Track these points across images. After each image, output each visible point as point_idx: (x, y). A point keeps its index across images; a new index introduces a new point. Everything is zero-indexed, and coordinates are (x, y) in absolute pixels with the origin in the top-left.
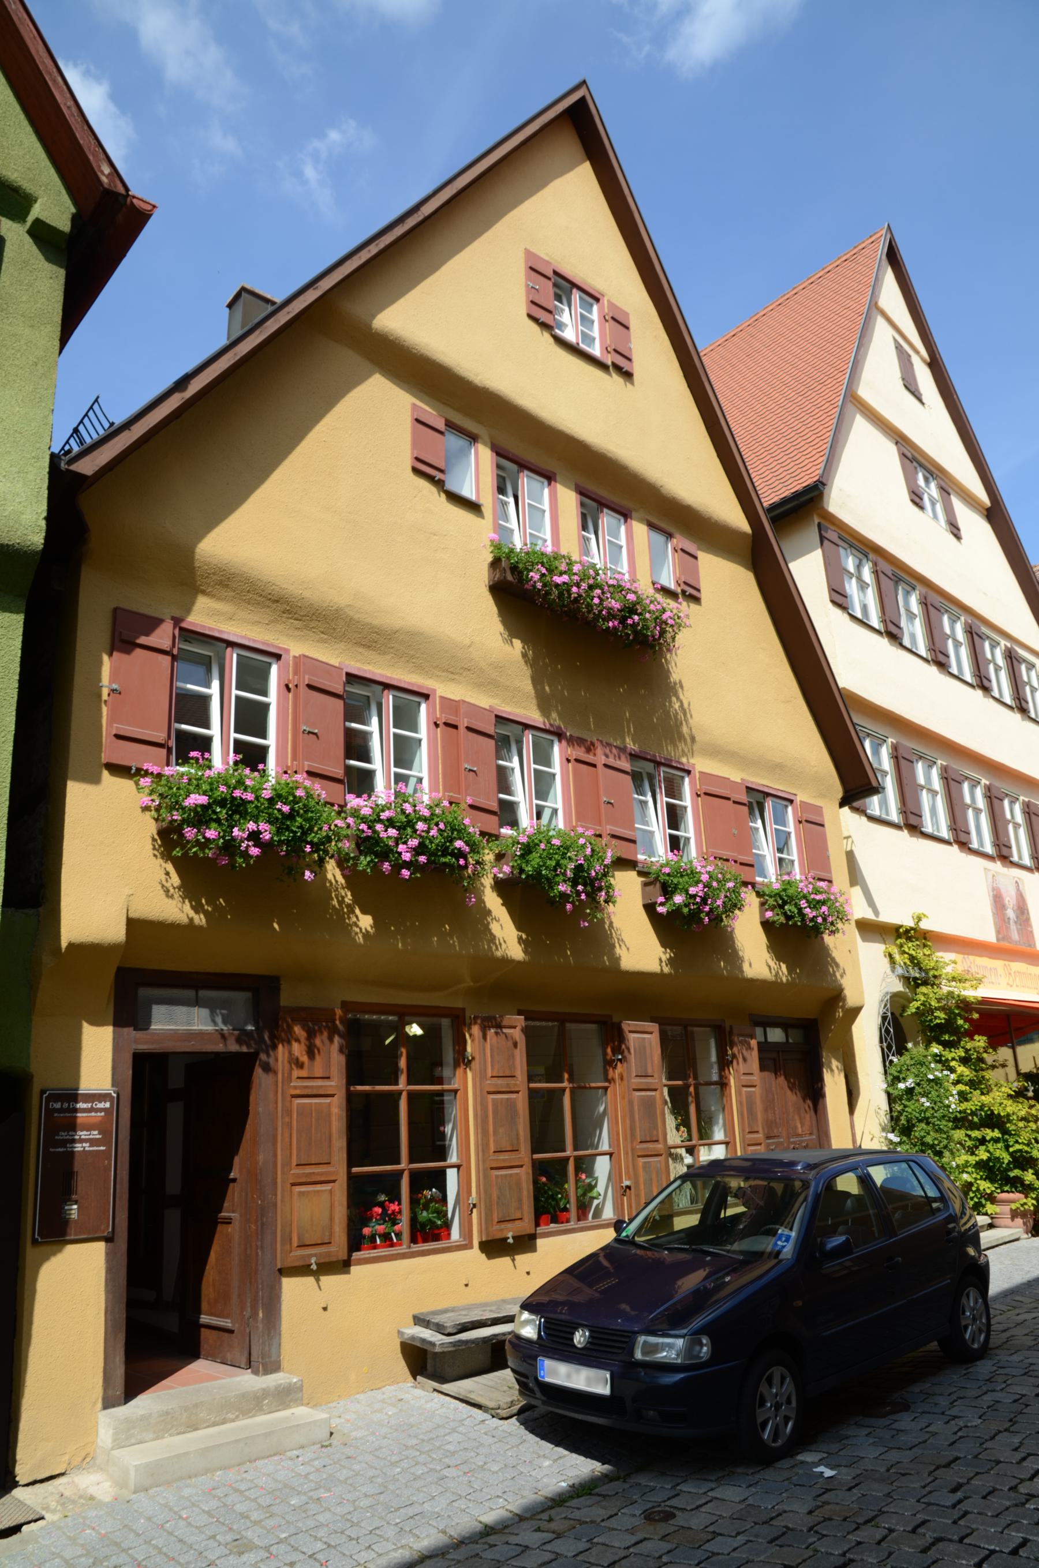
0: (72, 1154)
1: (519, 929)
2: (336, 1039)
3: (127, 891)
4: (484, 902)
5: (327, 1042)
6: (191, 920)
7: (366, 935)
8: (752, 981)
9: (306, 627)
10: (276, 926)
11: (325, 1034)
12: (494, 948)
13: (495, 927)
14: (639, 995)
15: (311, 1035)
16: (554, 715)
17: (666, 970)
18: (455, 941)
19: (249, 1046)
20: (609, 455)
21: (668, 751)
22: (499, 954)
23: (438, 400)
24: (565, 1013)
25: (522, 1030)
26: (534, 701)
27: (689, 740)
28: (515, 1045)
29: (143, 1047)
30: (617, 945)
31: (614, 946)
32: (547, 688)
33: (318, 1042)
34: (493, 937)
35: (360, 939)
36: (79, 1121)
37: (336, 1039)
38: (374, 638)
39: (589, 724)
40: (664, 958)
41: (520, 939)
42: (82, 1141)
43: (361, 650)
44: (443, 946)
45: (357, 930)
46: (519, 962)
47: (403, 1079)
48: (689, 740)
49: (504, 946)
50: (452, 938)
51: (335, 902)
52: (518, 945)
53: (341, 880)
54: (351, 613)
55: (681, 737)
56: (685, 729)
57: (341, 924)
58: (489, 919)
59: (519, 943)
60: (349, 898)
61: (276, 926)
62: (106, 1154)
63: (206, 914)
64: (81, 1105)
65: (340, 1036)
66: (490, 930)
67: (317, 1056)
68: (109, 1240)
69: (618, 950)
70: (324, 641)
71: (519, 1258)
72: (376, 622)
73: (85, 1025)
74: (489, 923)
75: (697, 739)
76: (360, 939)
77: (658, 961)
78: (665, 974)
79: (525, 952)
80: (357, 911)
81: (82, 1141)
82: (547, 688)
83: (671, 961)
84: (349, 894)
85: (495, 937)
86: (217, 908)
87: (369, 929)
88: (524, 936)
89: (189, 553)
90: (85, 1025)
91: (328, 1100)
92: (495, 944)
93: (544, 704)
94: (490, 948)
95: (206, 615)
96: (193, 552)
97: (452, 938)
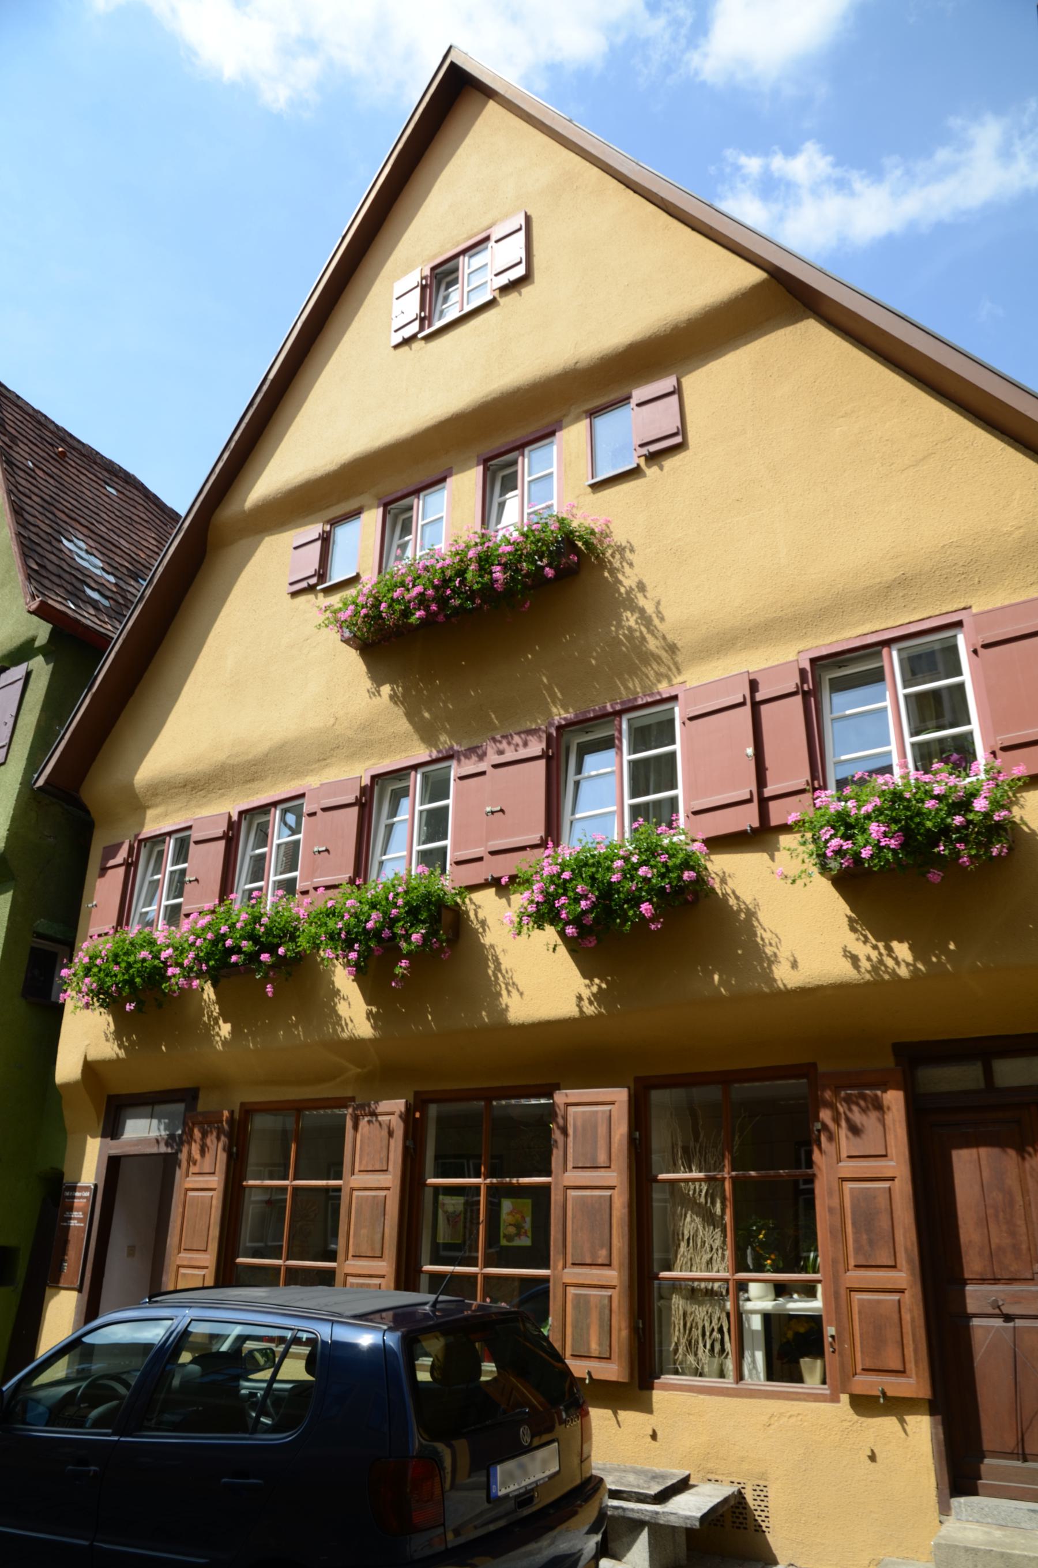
0: (68, 1227)
1: (368, 1003)
2: (223, 1138)
3: (87, 1043)
4: (333, 983)
5: (215, 1141)
6: (117, 1055)
7: (225, 1043)
8: (804, 992)
9: (209, 792)
10: (163, 1048)
11: (215, 1134)
12: (339, 1030)
13: (342, 1008)
14: (565, 1054)
15: (204, 1135)
16: (443, 738)
17: (590, 1010)
18: (300, 1031)
19: (172, 1148)
20: (489, 398)
21: (634, 689)
22: (345, 1035)
23: (320, 510)
24: (509, 1087)
25: (400, 1116)
26: (416, 737)
27: (664, 655)
28: (391, 1134)
29: (114, 1152)
30: (504, 993)
31: (500, 995)
32: (427, 715)
33: (208, 1141)
34: (339, 1017)
35: (219, 1047)
36: (75, 1205)
37: (223, 1138)
38: (253, 770)
39: (491, 722)
40: (586, 993)
41: (369, 1015)
42: (75, 1219)
43: (248, 786)
44: (292, 1036)
45: (218, 1038)
46: (370, 1040)
47: (726, 1170)
48: (664, 655)
49: (350, 1025)
50: (297, 1029)
51: (206, 1019)
52: (367, 1022)
53: (213, 997)
54: (231, 762)
55: (648, 658)
56: (653, 644)
57: (208, 1034)
58: (336, 1000)
59: (368, 1019)
60: (216, 1010)
61: (163, 1048)
62: (84, 1228)
63: (126, 1049)
64: (77, 1194)
65: (225, 1136)
66: (336, 1012)
67: (207, 1154)
68: (80, 1290)
69: (505, 999)
70: (223, 795)
71: (622, 1414)
72: (250, 757)
73: (89, 1138)
74: (335, 1004)
75: (679, 644)
76: (219, 1047)
77: (574, 1000)
78: (590, 1018)
79: (375, 1027)
80: (221, 1022)
81: (75, 1219)
82: (427, 715)
83: (599, 997)
84: (217, 1007)
85: (340, 1017)
86: (132, 1043)
87: (227, 1036)
88: (374, 1010)
89: (131, 786)
90: (89, 1138)
91: (210, 1193)
92: (341, 1025)
93: (427, 734)
94: (335, 1030)
95: (155, 824)
96: (132, 785)
97: (297, 1029)
